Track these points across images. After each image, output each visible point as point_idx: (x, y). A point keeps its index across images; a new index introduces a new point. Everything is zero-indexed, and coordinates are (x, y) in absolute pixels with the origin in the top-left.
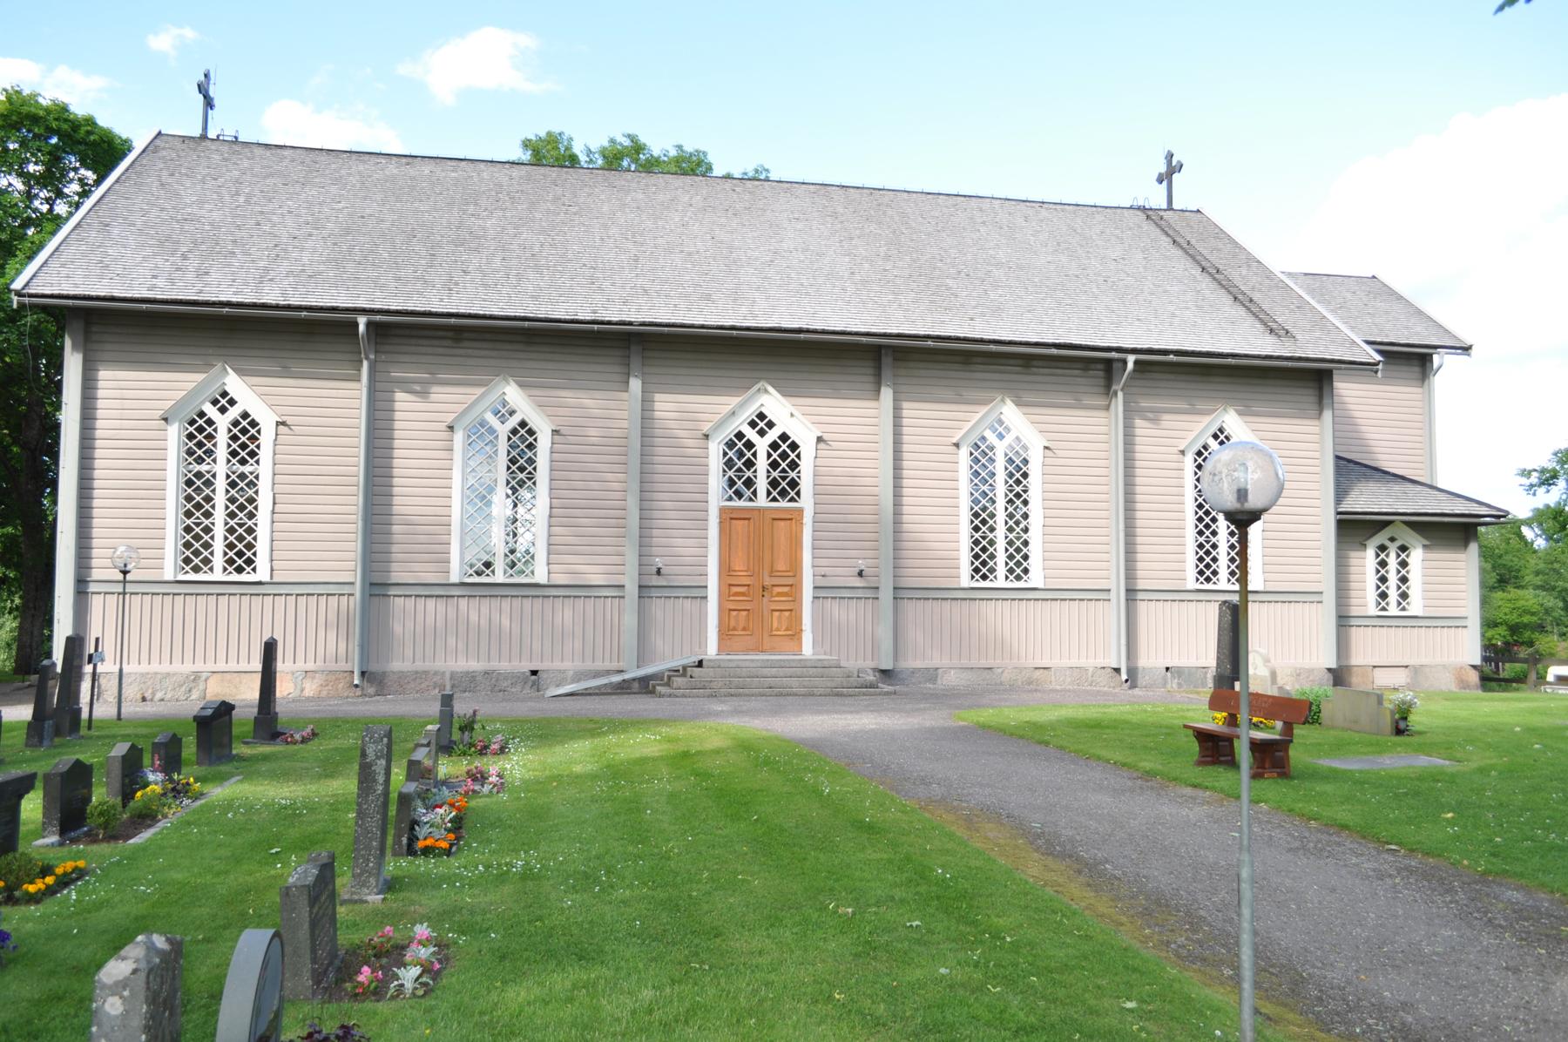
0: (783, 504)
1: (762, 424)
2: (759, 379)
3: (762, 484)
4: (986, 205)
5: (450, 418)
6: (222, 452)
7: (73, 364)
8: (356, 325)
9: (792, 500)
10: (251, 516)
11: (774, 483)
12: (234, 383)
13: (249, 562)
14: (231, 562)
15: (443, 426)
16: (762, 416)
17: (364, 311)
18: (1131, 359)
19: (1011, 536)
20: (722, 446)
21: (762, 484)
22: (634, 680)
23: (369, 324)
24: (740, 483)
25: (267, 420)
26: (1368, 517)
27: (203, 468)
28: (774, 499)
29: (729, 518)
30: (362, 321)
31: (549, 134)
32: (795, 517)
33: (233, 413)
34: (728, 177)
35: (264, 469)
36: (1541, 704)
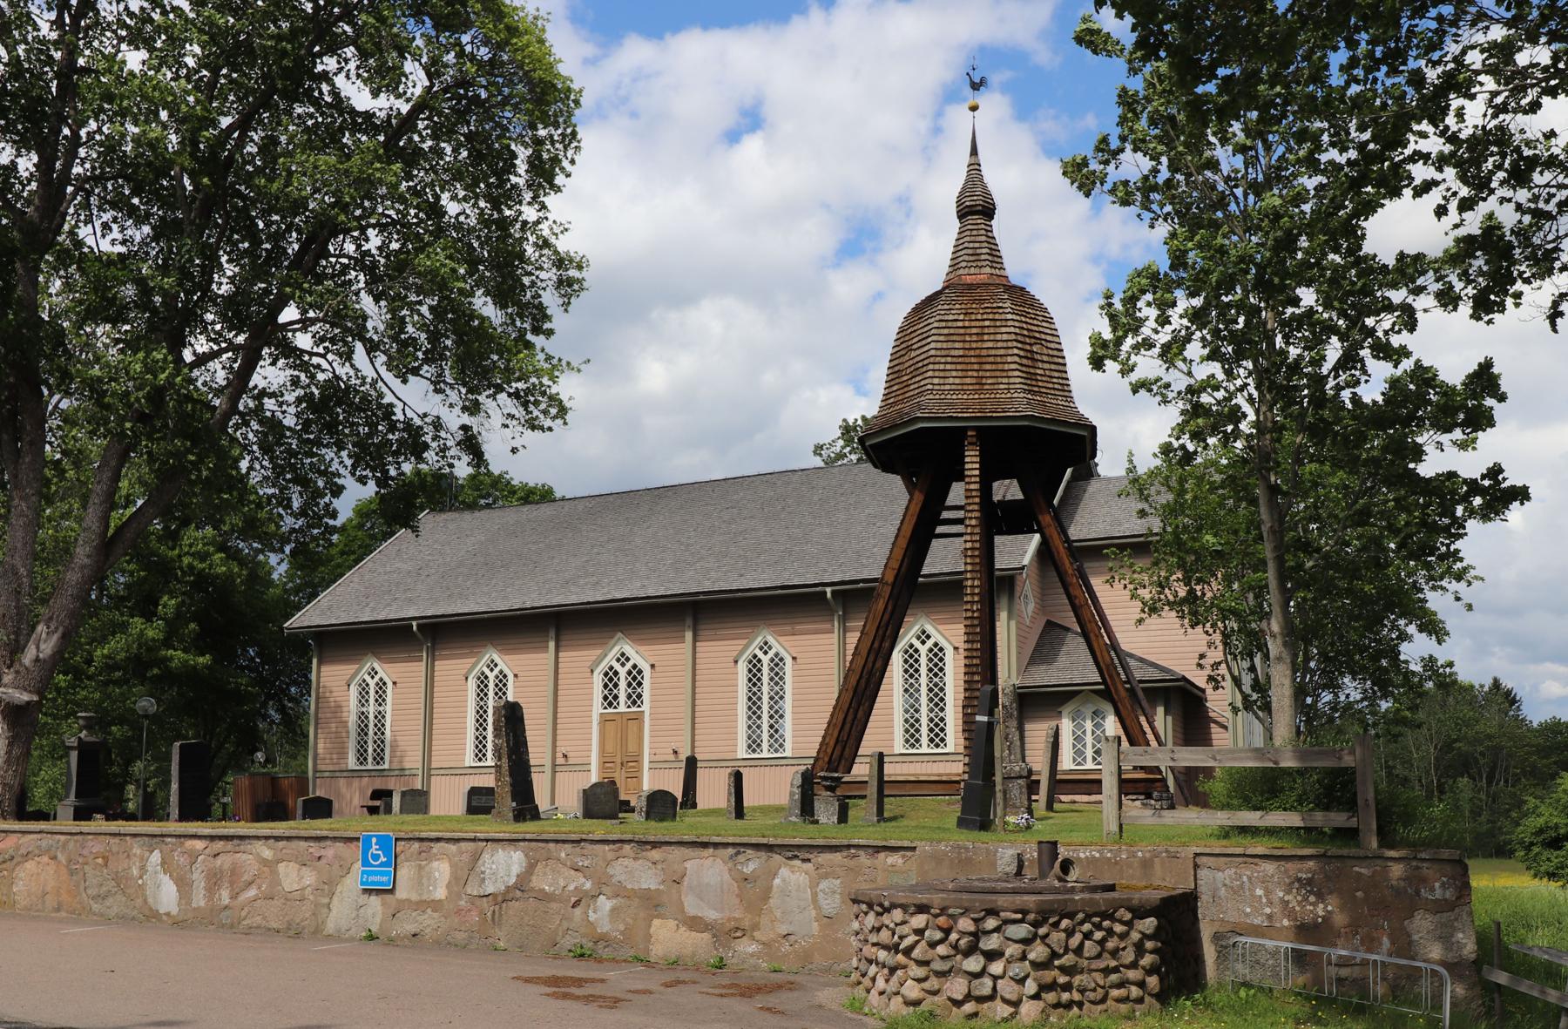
0: (634, 709)
2: (616, 632)
3: (622, 697)
5: (464, 672)
10: (942, 710)
13: (943, 740)
14: (931, 740)
15: (731, 659)
16: (623, 654)
18: (828, 590)
21: (622, 697)
22: (132, 817)
23: (418, 625)
24: (610, 700)
25: (645, 667)
29: (605, 720)
31: (1480, 364)
32: (638, 718)
33: (929, 643)
35: (388, 708)
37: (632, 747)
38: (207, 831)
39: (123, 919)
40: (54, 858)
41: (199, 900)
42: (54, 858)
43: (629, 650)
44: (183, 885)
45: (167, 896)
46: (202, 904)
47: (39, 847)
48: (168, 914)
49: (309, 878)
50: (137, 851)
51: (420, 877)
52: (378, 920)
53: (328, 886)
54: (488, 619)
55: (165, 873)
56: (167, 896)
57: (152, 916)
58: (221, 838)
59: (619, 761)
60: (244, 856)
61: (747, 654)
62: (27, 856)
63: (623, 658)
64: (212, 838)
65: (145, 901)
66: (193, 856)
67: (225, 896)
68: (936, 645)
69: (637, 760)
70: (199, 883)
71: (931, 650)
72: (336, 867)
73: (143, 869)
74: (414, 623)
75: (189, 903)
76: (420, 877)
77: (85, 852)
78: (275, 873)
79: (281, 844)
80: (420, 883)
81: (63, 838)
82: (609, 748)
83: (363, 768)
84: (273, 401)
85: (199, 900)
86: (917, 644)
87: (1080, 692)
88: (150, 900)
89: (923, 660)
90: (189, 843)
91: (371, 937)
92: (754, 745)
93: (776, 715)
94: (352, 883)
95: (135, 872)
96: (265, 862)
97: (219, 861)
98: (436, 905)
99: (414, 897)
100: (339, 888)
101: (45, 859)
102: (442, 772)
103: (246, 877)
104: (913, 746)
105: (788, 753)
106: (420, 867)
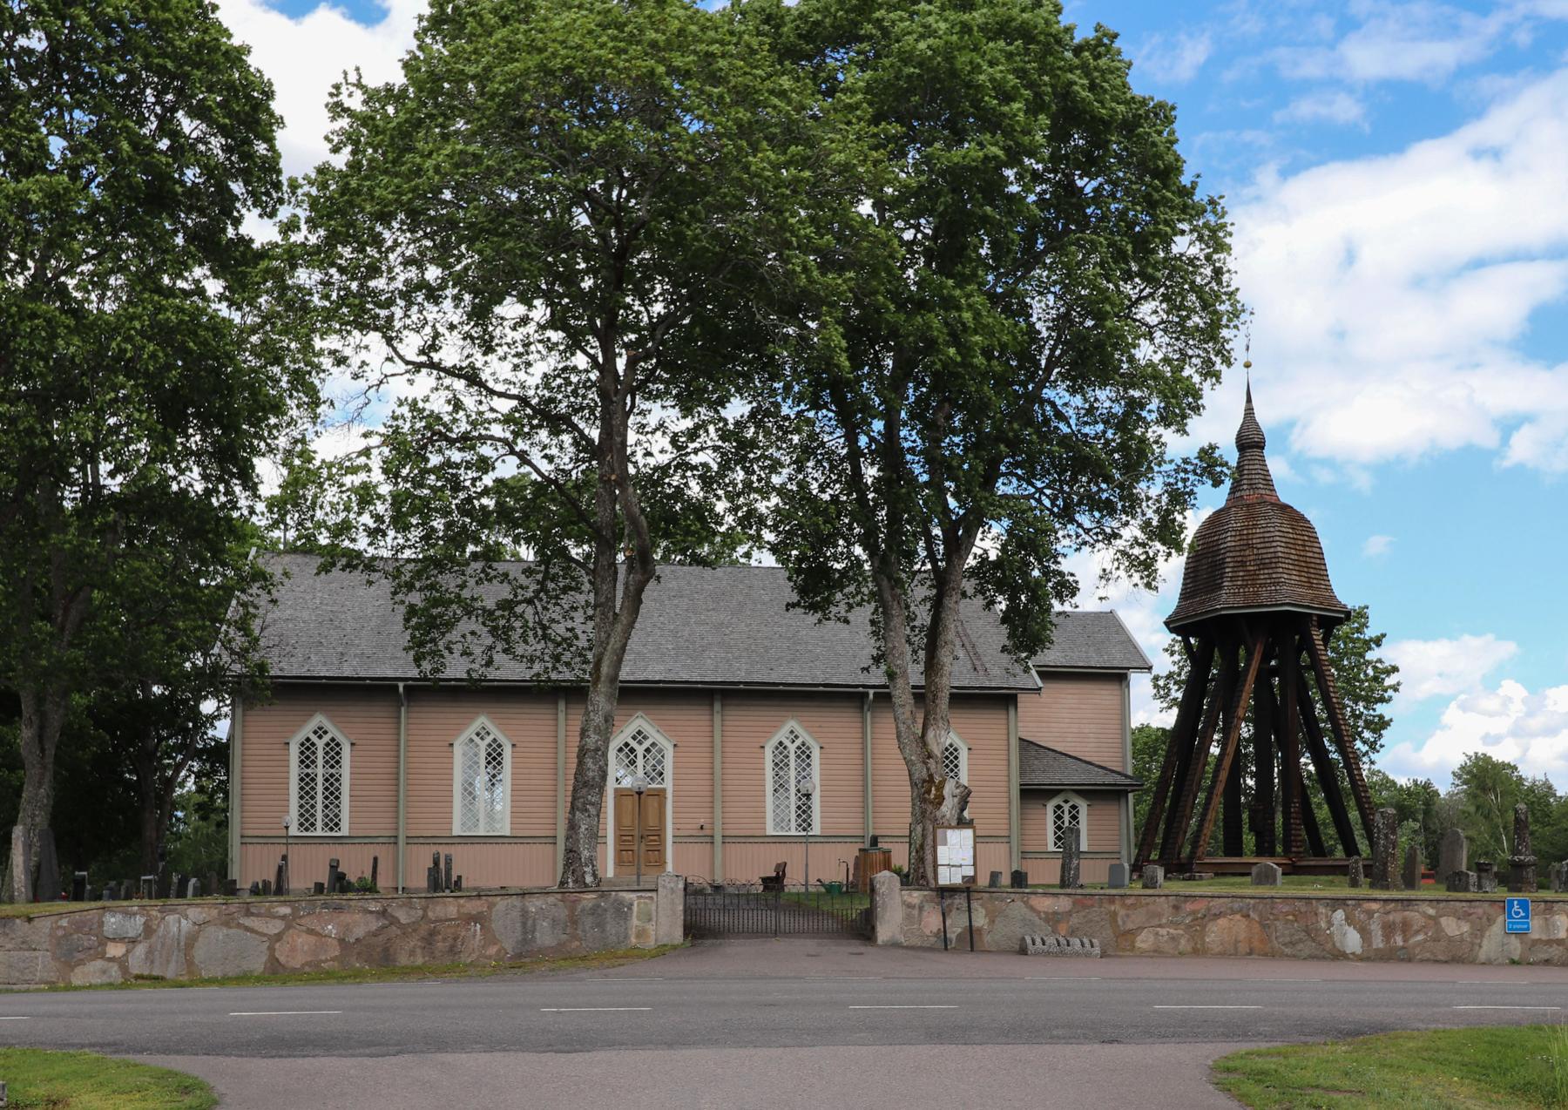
8: (397, 687)
16: (639, 733)
18: (871, 692)
23: (405, 687)
27: (309, 771)
30: (401, 685)
37: (652, 821)
38: (1384, 897)
39: (1313, 957)
40: (1248, 916)
41: (1378, 942)
42: (1248, 916)
43: (648, 729)
44: (1364, 932)
45: (1352, 940)
46: (1381, 946)
47: (1231, 908)
48: (1353, 954)
49: (1466, 927)
50: (1322, 910)
51: (1547, 925)
52: (1519, 952)
53: (1479, 932)
54: (498, 687)
55: (1349, 925)
56: (1352, 940)
57: (1339, 956)
58: (1393, 900)
59: (636, 833)
60: (1413, 914)
61: (300, 736)
62: (1217, 916)
63: (639, 736)
64: (1386, 901)
65: (1334, 945)
66: (1370, 914)
67: (1399, 941)
68: (495, 740)
69: (659, 834)
70: (1376, 928)
71: (327, 744)
72: (1485, 919)
73: (1330, 924)
74: (401, 685)
75: (1370, 945)
76: (1547, 925)
77: (1275, 911)
78: (1437, 923)
79: (1442, 905)
80: (1548, 929)
81: (1252, 901)
82: (627, 821)
83: (333, 834)
84: (347, 103)
85: (1378, 942)
86: (314, 738)
87: (1062, 791)
88: (1338, 945)
89: (320, 753)
90: (1367, 905)
91: (1513, 962)
92: (307, 821)
93: (332, 794)
94: (1496, 929)
95: (1323, 925)
96: (1430, 917)
97: (1391, 917)
98: (1560, 942)
99: (1544, 937)
100: (1487, 934)
101: (1238, 917)
102: (421, 841)
103: (1415, 927)
104: (804, 830)
105: (345, 830)
106: (1546, 919)
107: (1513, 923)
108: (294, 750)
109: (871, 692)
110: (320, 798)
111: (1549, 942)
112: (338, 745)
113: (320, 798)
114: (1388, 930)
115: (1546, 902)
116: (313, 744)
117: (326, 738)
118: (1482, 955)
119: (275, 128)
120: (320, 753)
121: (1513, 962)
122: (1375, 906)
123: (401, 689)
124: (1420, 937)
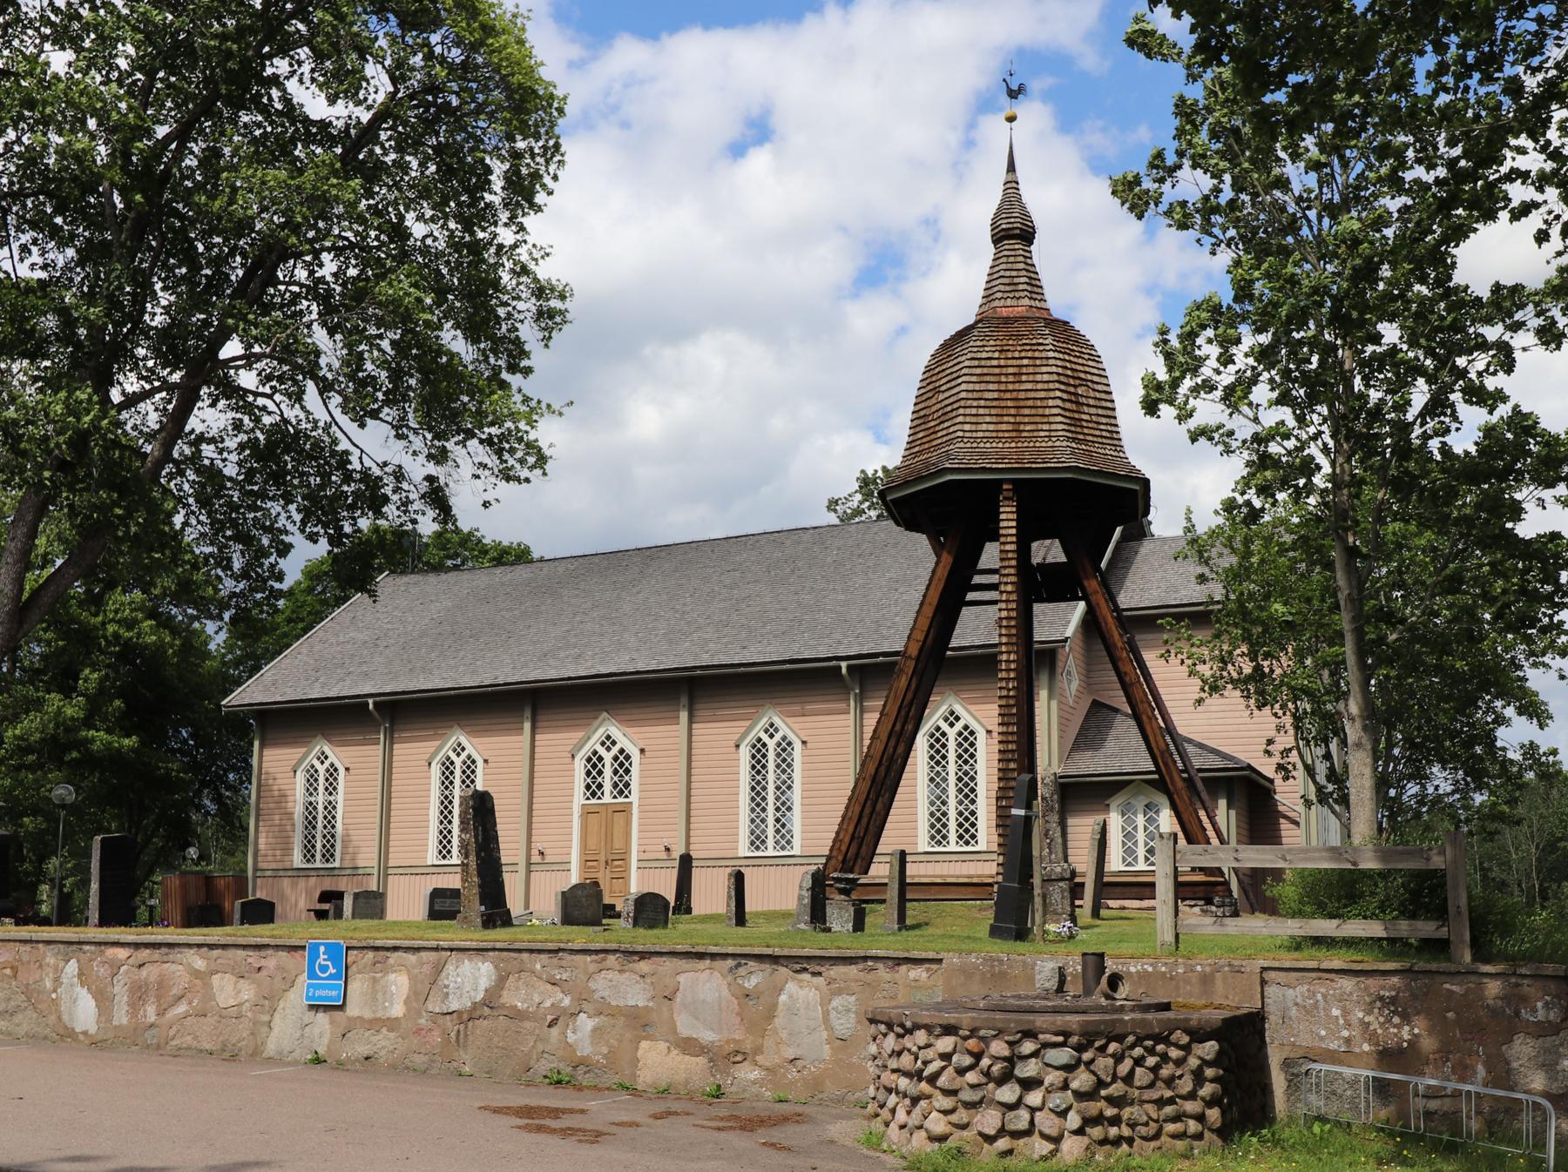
0: (621, 800)
1: (608, 743)
3: (607, 787)
4: (806, 536)
6: (321, 789)
7: (256, 743)
8: (840, 668)
9: (626, 797)
10: (973, 802)
11: (615, 785)
12: (615, 731)
13: (789, 842)
14: (961, 837)
15: (732, 743)
16: (608, 737)
17: (371, 695)
18: (844, 665)
19: (961, 808)
20: (584, 761)
21: (607, 787)
22: (45, 922)
23: (375, 704)
24: (594, 790)
26: (1088, 779)
27: (332, 798)
28: (615, 797)
29: (587, 812)
30: (371, 701)
32: (625, 810)
34: (541, 560)
35: (340, 797)
36: (160, 937)
39: (33, 1038)
41: (121, 1017)
46: (125, 1021)
48: (85, 1033)
50: (51, 960)
51: (374, 992)
52: (326, 1041)
56: (83, 1012)
58: (147, 945)
60: (173, 967)
61: (750, 738)
64: (137, 946)
65: (59, 1018)
66: (115, 967)
67: (150, 1013)
68: (966, 727)
70: (120, 992)
73: (57, 981)
74: (371, 701)
75: (110, 1021)
76: (374, 992)
78: (208, 986)
80: (375, 999)
84: (212, 447)
85: (121, 1017)
86: (945, 727)
88: (65, 1017)
89: (952, 745)
91: (318, 1061)
93: (784, 807)
95: (48, 984)
97: (144, 972)
98: (391, 1024)
99: (368, 1015)
100: (282, 1004)
106: (375, 980)
107: (316, 987)
108: (580, 766)
109: (844, 665)
110: (952, 814)
111: (376, 1024)
112: (972, 733)
113: (952, 814)
114: (139, 994)
115: (376, 949)
116: (944, 734)
117: (959, 726)
118: (271, 1048)
119: (388, 413)
120: (952, 745)
121: (318, 1061)
122: (122, 953)
123: (844, 671)
124: (182, 1008)
